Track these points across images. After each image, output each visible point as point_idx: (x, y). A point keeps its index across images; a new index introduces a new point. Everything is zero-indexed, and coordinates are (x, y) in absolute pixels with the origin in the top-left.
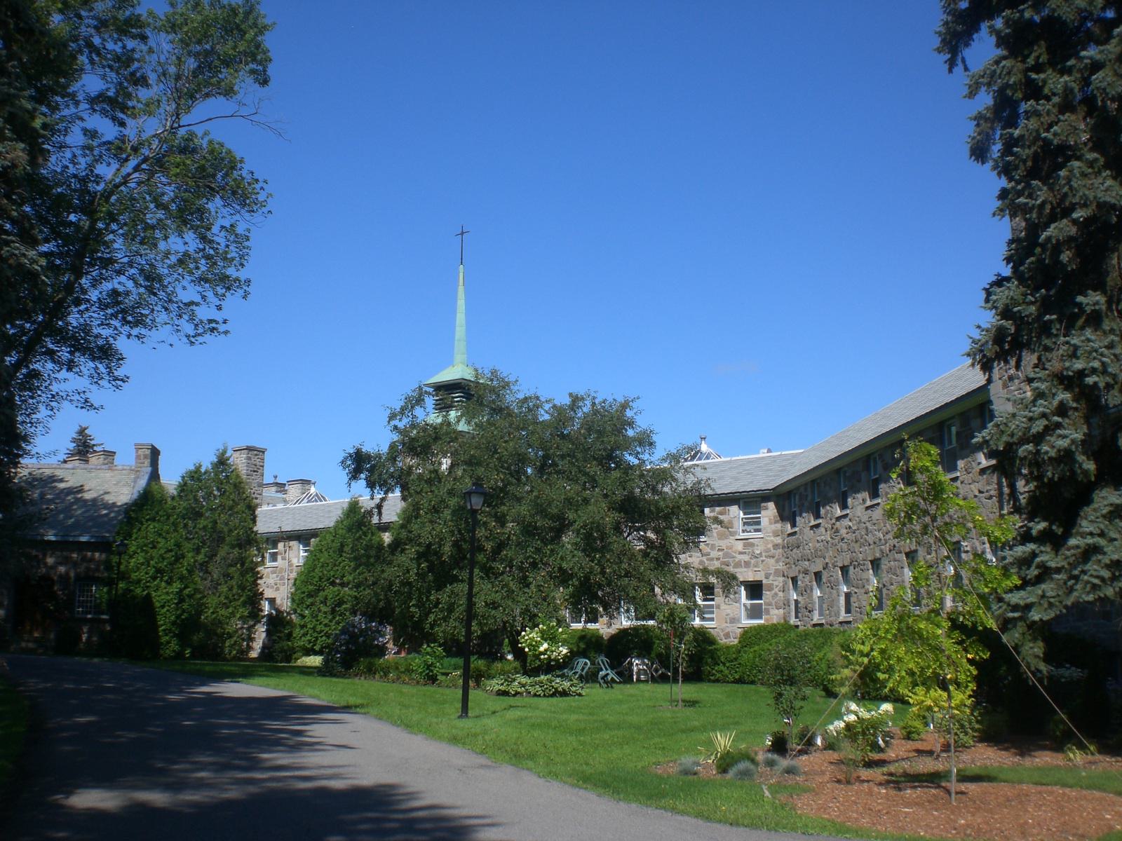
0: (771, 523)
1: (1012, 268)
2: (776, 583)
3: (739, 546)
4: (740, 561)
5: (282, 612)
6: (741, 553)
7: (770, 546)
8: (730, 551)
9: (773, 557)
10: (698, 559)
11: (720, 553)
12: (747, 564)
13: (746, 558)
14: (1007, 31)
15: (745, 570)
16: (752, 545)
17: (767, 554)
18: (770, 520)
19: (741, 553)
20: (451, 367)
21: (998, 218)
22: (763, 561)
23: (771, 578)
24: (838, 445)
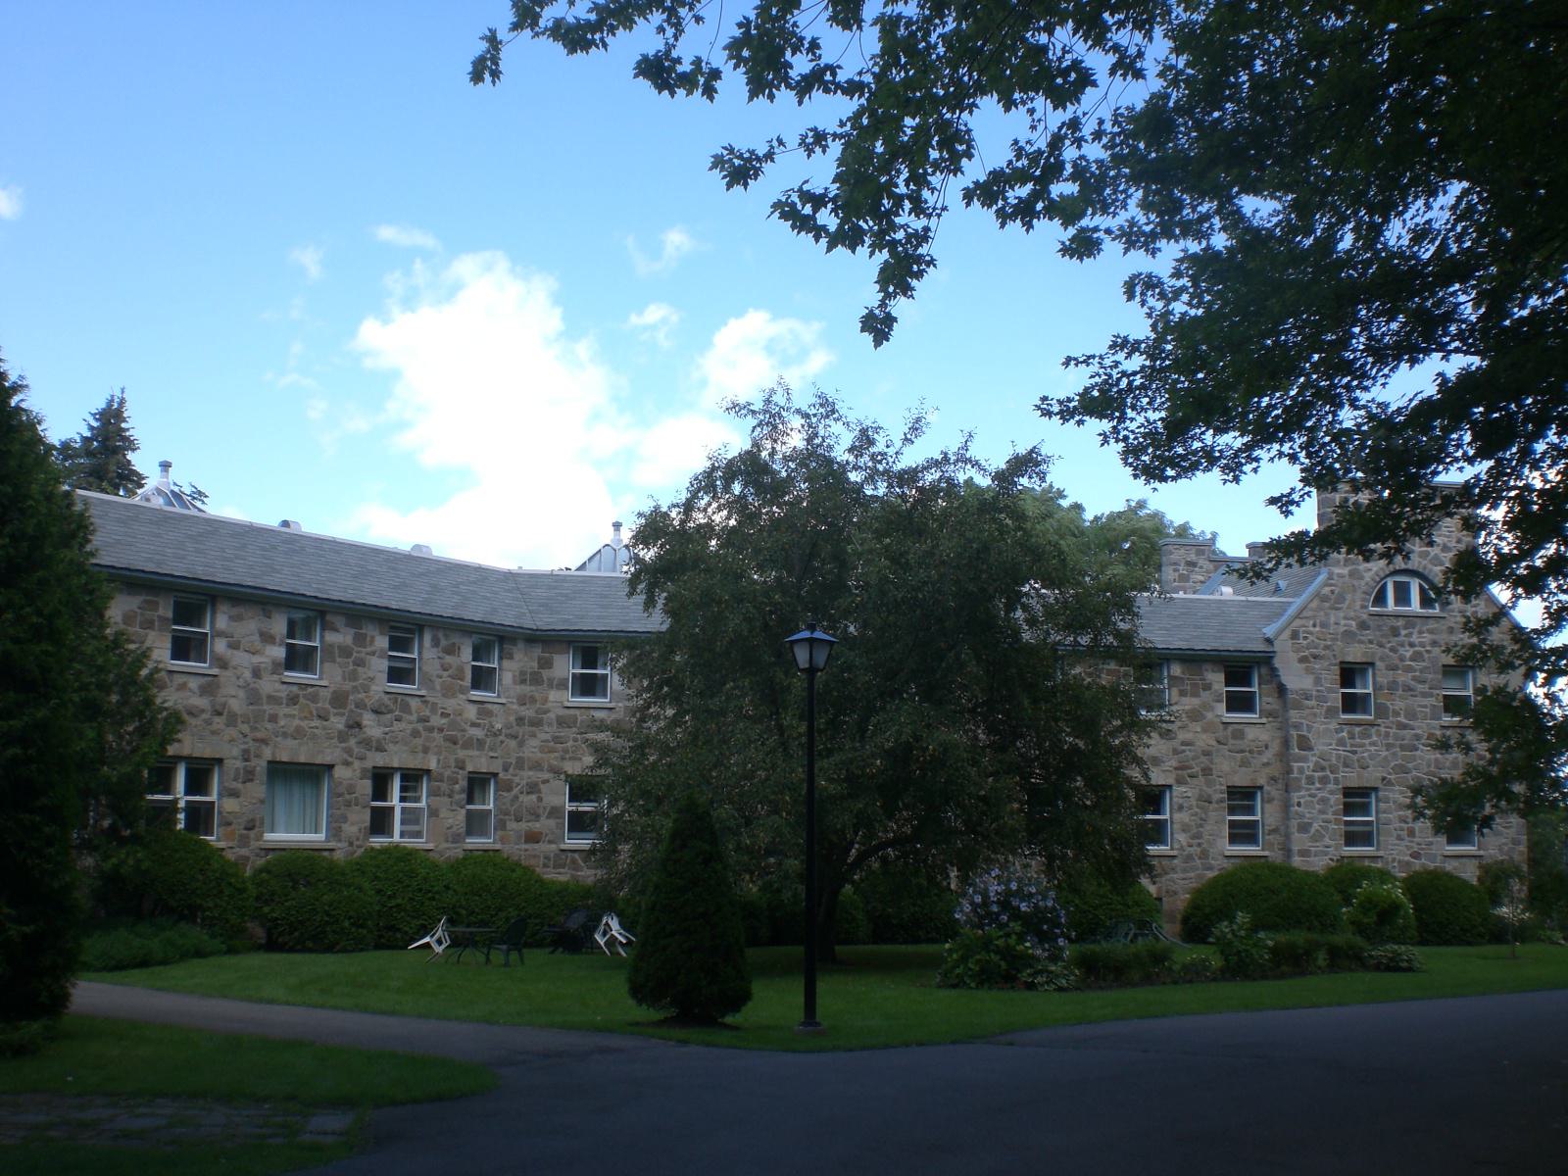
0: (515, 683)
1: (88, 541)
2: (517, 780)
3: (471, 712)
4: (471, 739)
5: (955, 486)
6: (473, 725)
7: (512, 719)
8: (459, 718)
9: (516, 737)
10: (410, 727)
11: (444, 721)
12: (481, 744)
13: (478, 733)
14: (1485, 363)
15: (476, 753)
16: (489, 714)
17: (508, 732)
18: (514, 676)
19: (473, 725)
20: (1089, 90)
21: (1065, 493)
22: (502, 742)
23: (511, 770)
24: (599, 617)
